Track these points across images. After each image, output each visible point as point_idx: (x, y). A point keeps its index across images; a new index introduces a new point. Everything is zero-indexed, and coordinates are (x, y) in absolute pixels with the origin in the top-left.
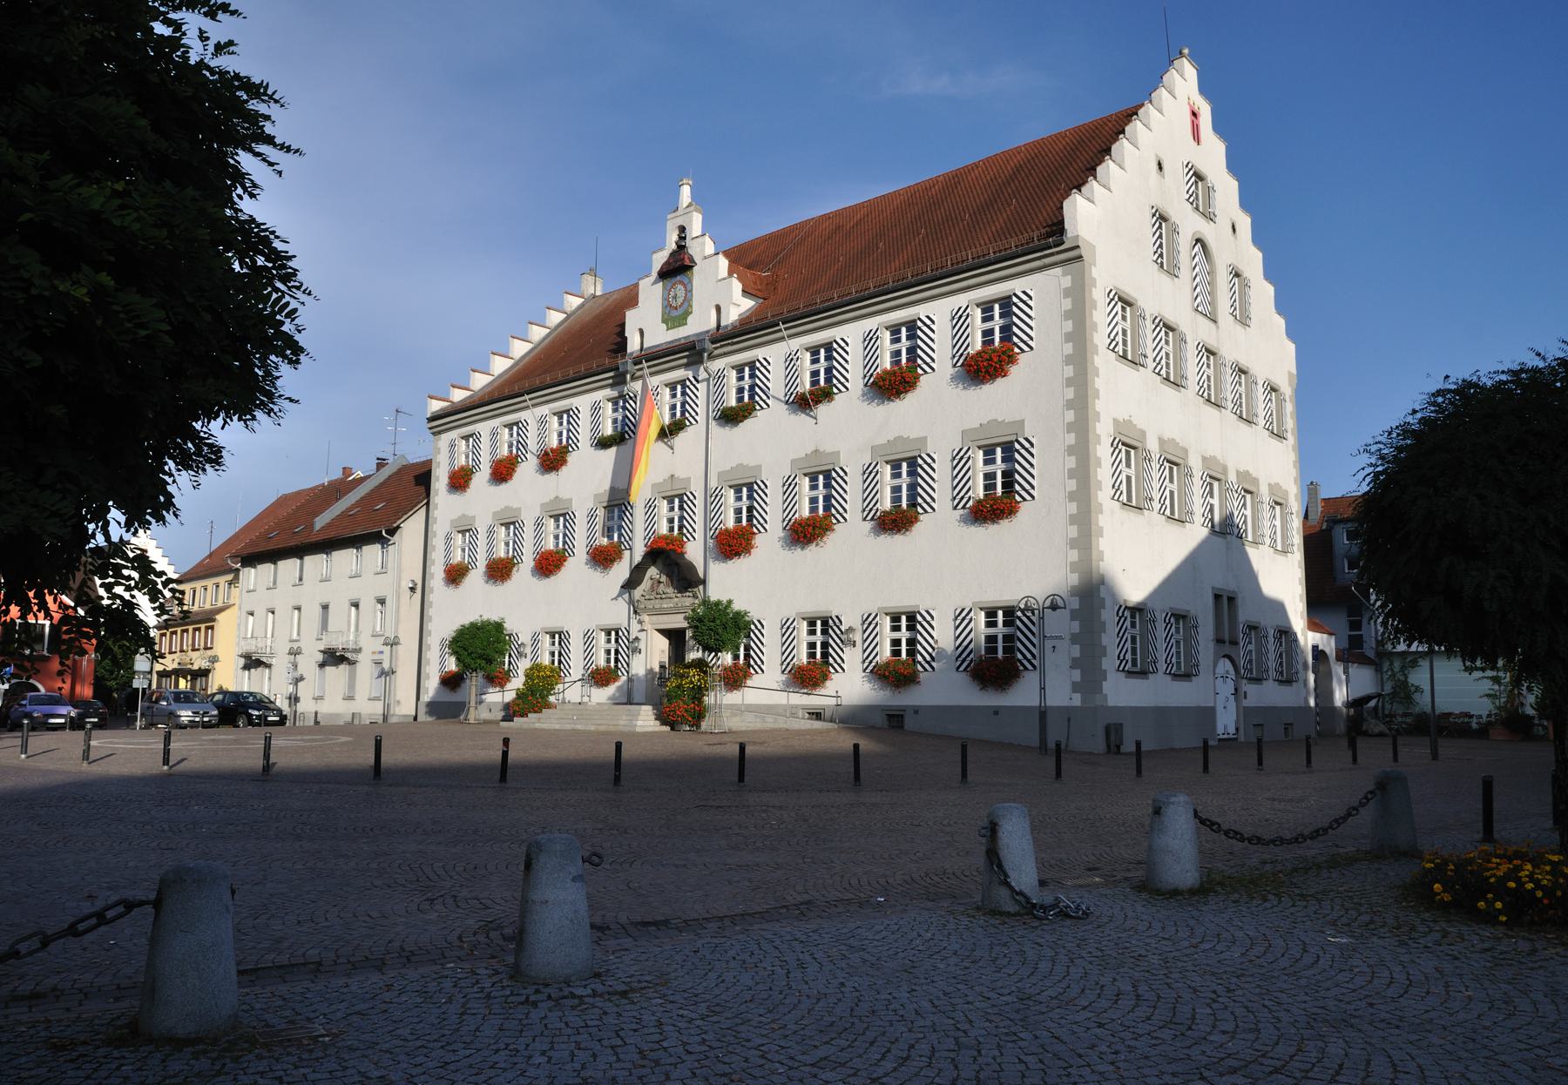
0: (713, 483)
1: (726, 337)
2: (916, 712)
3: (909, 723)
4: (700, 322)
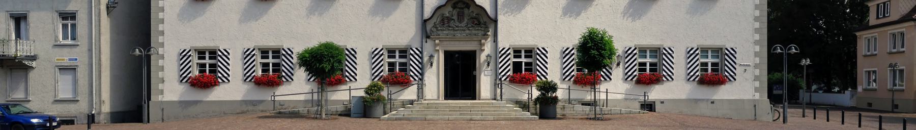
2: (662, 102)
3: (658, 107)
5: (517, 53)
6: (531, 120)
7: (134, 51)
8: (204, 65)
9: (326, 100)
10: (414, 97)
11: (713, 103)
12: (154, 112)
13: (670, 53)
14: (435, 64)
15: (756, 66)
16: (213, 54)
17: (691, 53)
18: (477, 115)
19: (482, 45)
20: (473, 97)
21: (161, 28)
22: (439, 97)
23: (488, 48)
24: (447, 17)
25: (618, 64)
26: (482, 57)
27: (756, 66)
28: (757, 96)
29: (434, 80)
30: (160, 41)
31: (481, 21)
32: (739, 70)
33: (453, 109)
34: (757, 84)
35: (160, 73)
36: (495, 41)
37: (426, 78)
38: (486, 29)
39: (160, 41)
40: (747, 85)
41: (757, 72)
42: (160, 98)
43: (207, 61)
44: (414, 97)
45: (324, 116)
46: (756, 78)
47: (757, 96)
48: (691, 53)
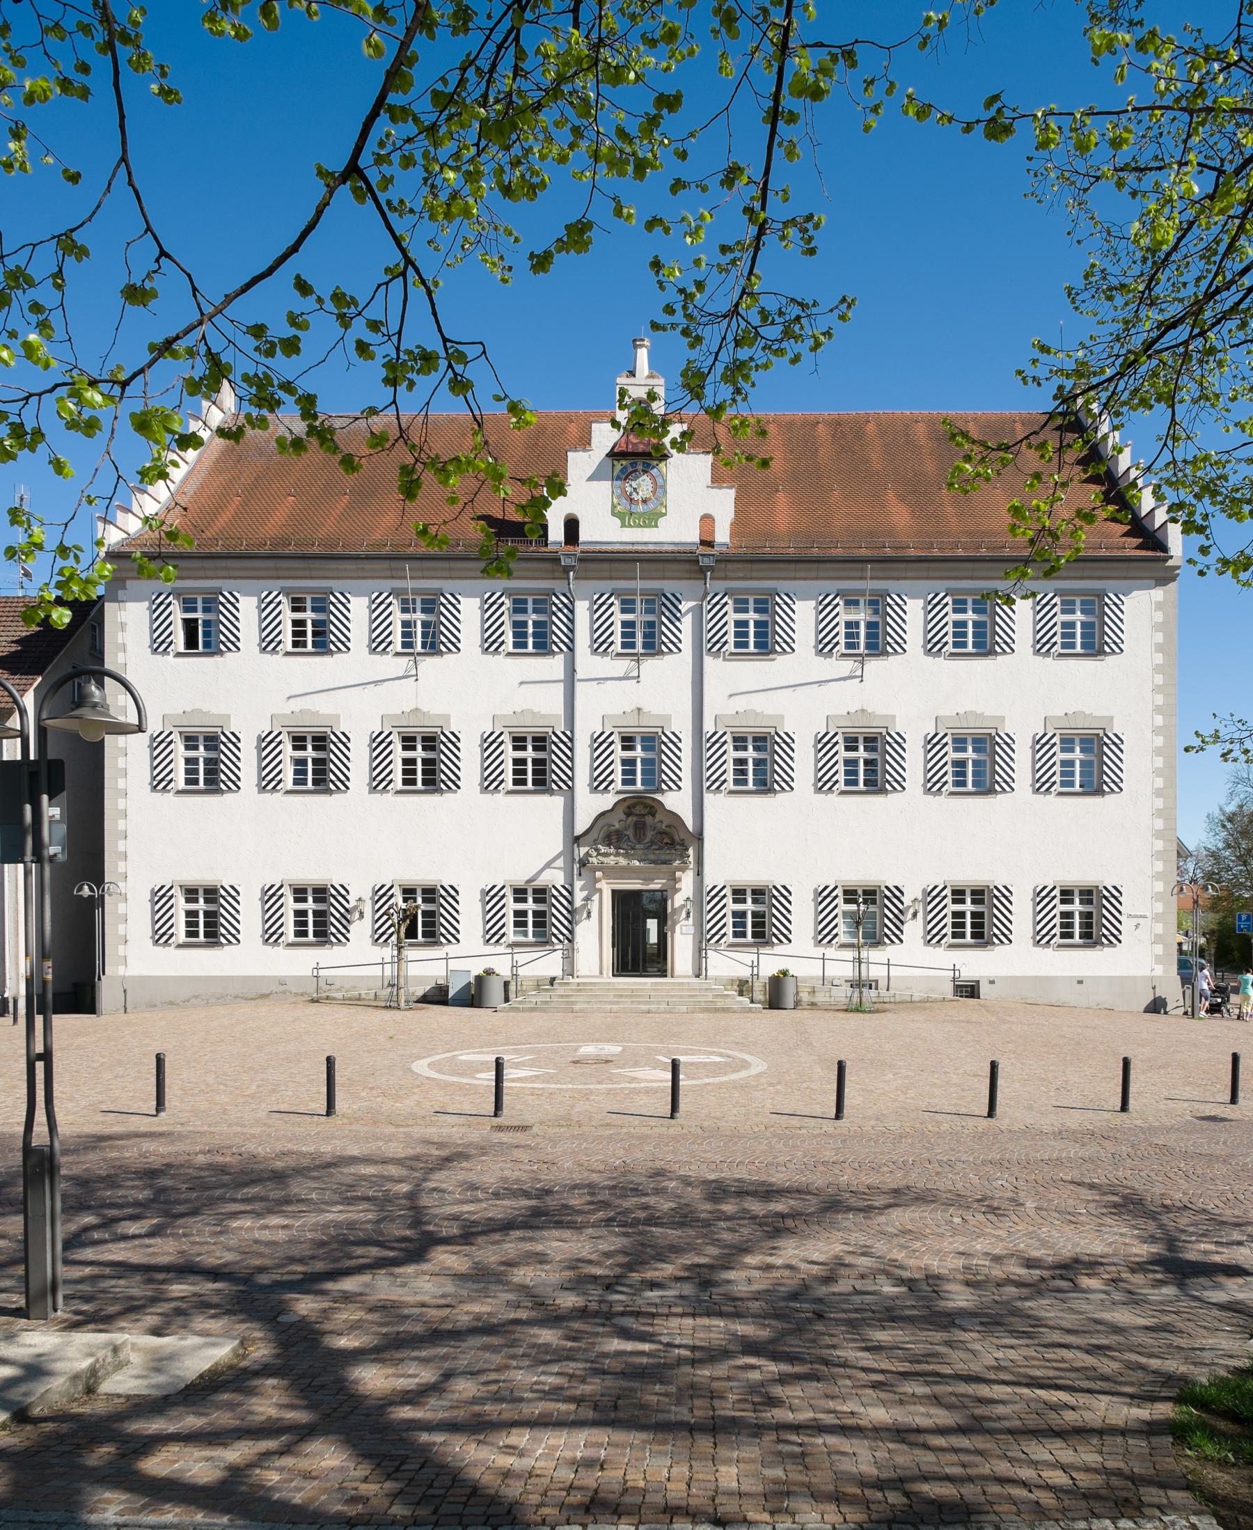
0: (709, 727)
1: (691, 563)
2: (992, 982)
3: (984, 989)
4: (676, 529)
5: (739, 895)
6: (750, 1010)
7: (80, 889)
8: (854, 762)
9: (406, 977)
10: (558, 972)
11: (1080, 982)
12: (107, 992)
13: (1006, 894)
14: (595, 914)
15: (1157, 918)
16: (212, 894)
17: (1040, 895)
18: (659, 1003)
19: (676, 880)
20: (663, 973)
21: (121, 848)
22: (601, 973)
23: (687, 882)
24: (617, 831)
25: (915, 915)
26: (678, 900)
27: (1157, 918)
28: (1159, 971)
29: (594, 940)
30: (121, 807)
31: (676, 838)
32: (1126, 926)
33: (633, 994)
34: (1159, 949)
35: (121, 948)
36: (699, 873)
37: (579, 938)
38: (683, 856)
39: (121, 807)
40: (1144, 951)
41: (1159, 928)
42: (121, 971)
43: (638, 753)
44: (558, 972)
45: (403, 1005)
46: (1158, 939)
47: (1159, 971)
48: (1040, 895)
